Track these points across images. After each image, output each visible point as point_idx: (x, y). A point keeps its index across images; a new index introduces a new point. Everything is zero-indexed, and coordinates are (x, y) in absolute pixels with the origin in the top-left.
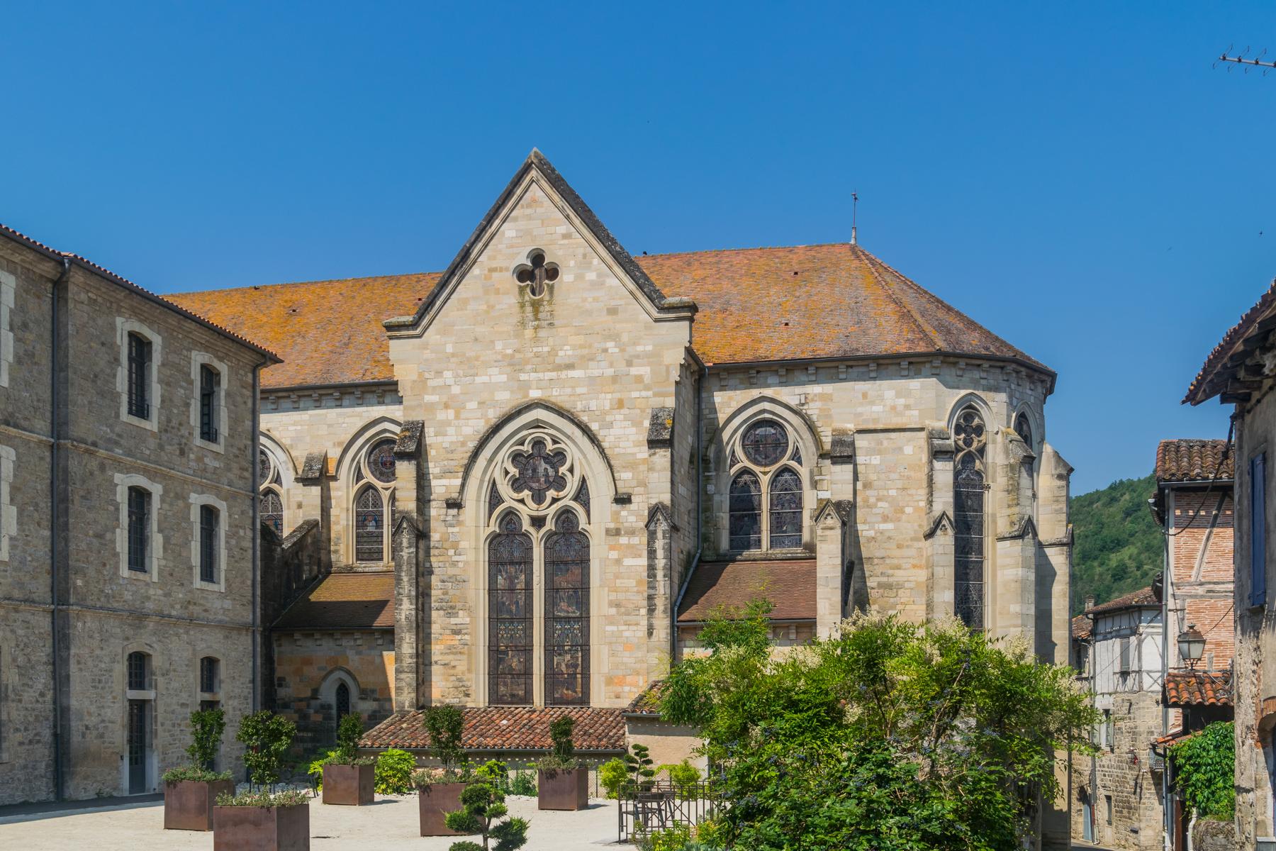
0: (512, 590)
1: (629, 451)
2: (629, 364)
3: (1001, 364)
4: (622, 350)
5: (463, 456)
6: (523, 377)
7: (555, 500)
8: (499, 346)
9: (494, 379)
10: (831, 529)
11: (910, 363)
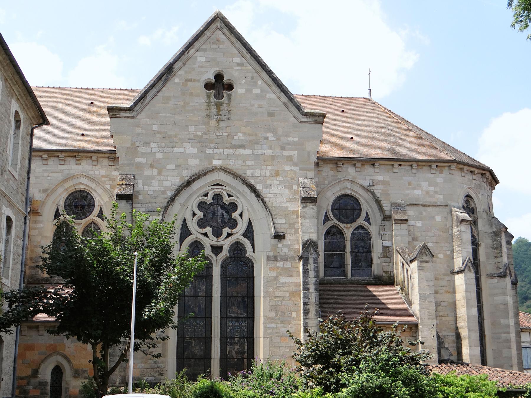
0: (196, 296)
1: (284, 205)
2: (283, 148)
3: (483, 172)
4: (278, 139)
5: (163, 201)
6: (209, 151)
7: (229, 235)
8: (192, 129)
9: (188, 151)
10: (427, 262)
11: (400, 165)
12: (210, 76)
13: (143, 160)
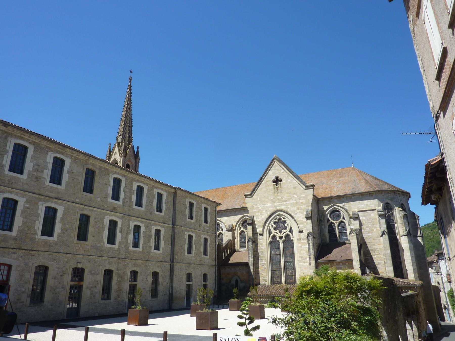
2: (300, 199)
4: (298, 197)
6: (275, 204)
7: (284, 232)
8: (269, 198)
12: (274, 178)
13: (256, 210)
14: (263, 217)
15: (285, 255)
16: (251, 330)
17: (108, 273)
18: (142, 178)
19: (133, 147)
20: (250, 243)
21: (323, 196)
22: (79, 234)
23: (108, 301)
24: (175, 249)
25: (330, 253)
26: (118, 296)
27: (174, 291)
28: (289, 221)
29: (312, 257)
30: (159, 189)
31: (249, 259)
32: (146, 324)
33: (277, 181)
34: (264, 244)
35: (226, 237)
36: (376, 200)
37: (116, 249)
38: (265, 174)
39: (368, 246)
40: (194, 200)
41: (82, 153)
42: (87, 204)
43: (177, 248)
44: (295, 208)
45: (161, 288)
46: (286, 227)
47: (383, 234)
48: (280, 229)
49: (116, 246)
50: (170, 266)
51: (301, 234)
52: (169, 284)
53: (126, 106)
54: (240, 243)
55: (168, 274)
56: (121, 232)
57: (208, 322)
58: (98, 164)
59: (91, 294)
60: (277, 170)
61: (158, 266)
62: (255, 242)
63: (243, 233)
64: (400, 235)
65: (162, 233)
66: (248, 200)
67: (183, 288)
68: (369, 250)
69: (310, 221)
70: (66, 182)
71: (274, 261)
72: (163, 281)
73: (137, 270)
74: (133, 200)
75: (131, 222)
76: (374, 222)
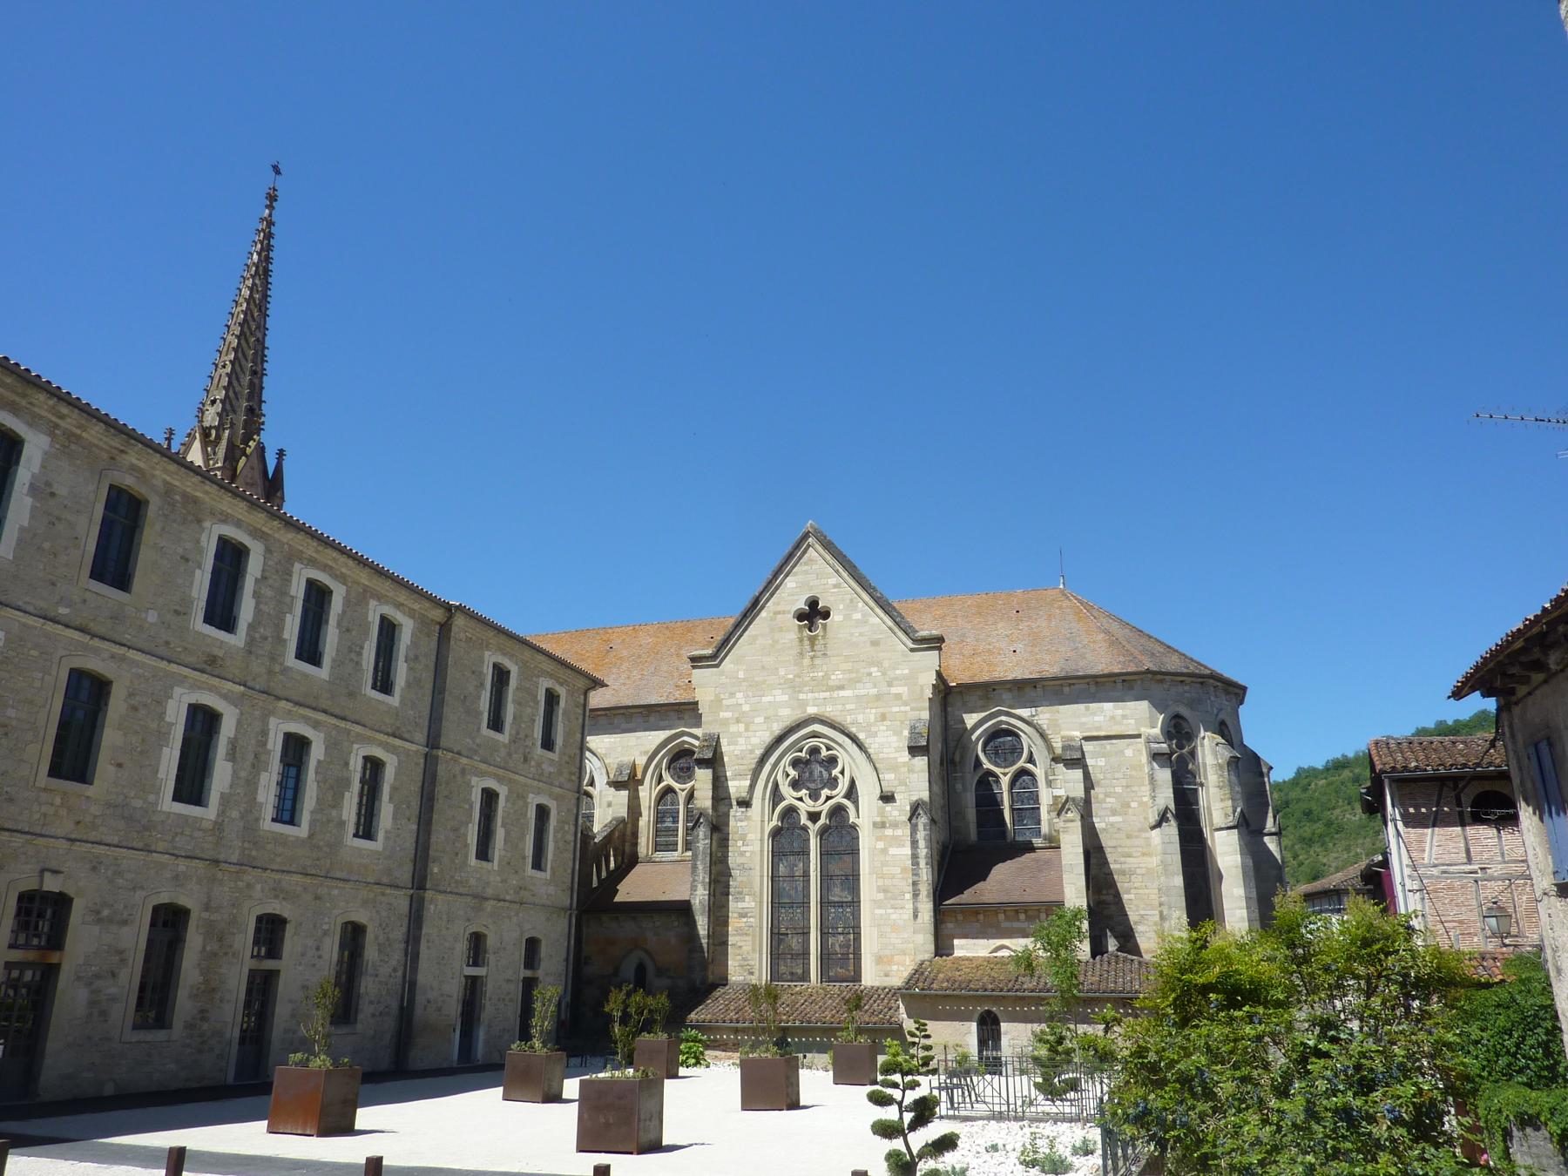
2: (890, 684)
4: (884, 674)
6: (801, 696)
7: (828, 798)
8: (782, 672)
12: (801, 604)
13: (728, 715)
14: (755, 741)
15: (825, 877)
16: (921, 1155)
17: (170, 922)
18: (329, 551)
19: (261, 449)
20: (702, 832)
21: (965, 678)
22: (58, 753)
23: (161, 1035)
24: (433, 839)
25: (983, 876)
26: (203, 1014)
27: (420, 999)
28: (848, 758)
29: (925, 889)
30: (387, 603)
31: (693, 888)
32: (348, 1129)
33: (813, 614)
34: (750, 836)
35: (607, 808)
36: (1145, 704)
37: (207, 825)
38: (771, 585)
39: (1110, 858)
40: (511, 657)
41: (100, 420)
42: (102, 630)
43: (439, 837)
44: (872, 715)
45: (368, 986)
46: (836, 779)
47: (1162, 819)
48: (812, 786)
49: (209, 813)
50: (407, 903)
51: (888, 807)
52: (400, 973)
53: (246, 293)
54: (657, 832)
55: (399, 933)
56: (232, 756)
57: (622, 1123)
58: (163, 474)
59: (92, 1003)
60: (814, 576)
61: (365, 903)
62: (719, 829)
63: (669, 797)
64: (1212, 824)
65: (389, 774)
66: (700, 675)
67: (453, 990)
68: (1111, 874)
69: (921, 762)
70: (22, 529)
71: (785, 900)
72: (382, 961)
73: (285, 915)
74: (286, 635)
75: (273, 721)
76: (1131, 777)
